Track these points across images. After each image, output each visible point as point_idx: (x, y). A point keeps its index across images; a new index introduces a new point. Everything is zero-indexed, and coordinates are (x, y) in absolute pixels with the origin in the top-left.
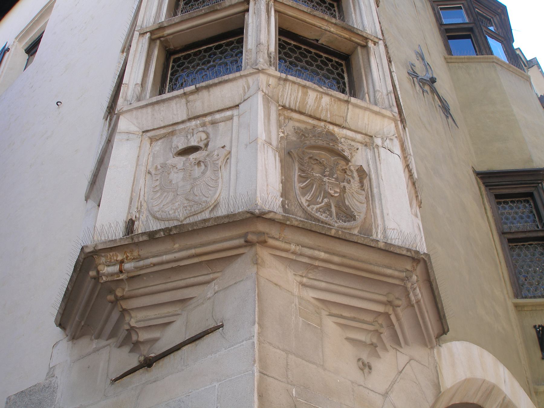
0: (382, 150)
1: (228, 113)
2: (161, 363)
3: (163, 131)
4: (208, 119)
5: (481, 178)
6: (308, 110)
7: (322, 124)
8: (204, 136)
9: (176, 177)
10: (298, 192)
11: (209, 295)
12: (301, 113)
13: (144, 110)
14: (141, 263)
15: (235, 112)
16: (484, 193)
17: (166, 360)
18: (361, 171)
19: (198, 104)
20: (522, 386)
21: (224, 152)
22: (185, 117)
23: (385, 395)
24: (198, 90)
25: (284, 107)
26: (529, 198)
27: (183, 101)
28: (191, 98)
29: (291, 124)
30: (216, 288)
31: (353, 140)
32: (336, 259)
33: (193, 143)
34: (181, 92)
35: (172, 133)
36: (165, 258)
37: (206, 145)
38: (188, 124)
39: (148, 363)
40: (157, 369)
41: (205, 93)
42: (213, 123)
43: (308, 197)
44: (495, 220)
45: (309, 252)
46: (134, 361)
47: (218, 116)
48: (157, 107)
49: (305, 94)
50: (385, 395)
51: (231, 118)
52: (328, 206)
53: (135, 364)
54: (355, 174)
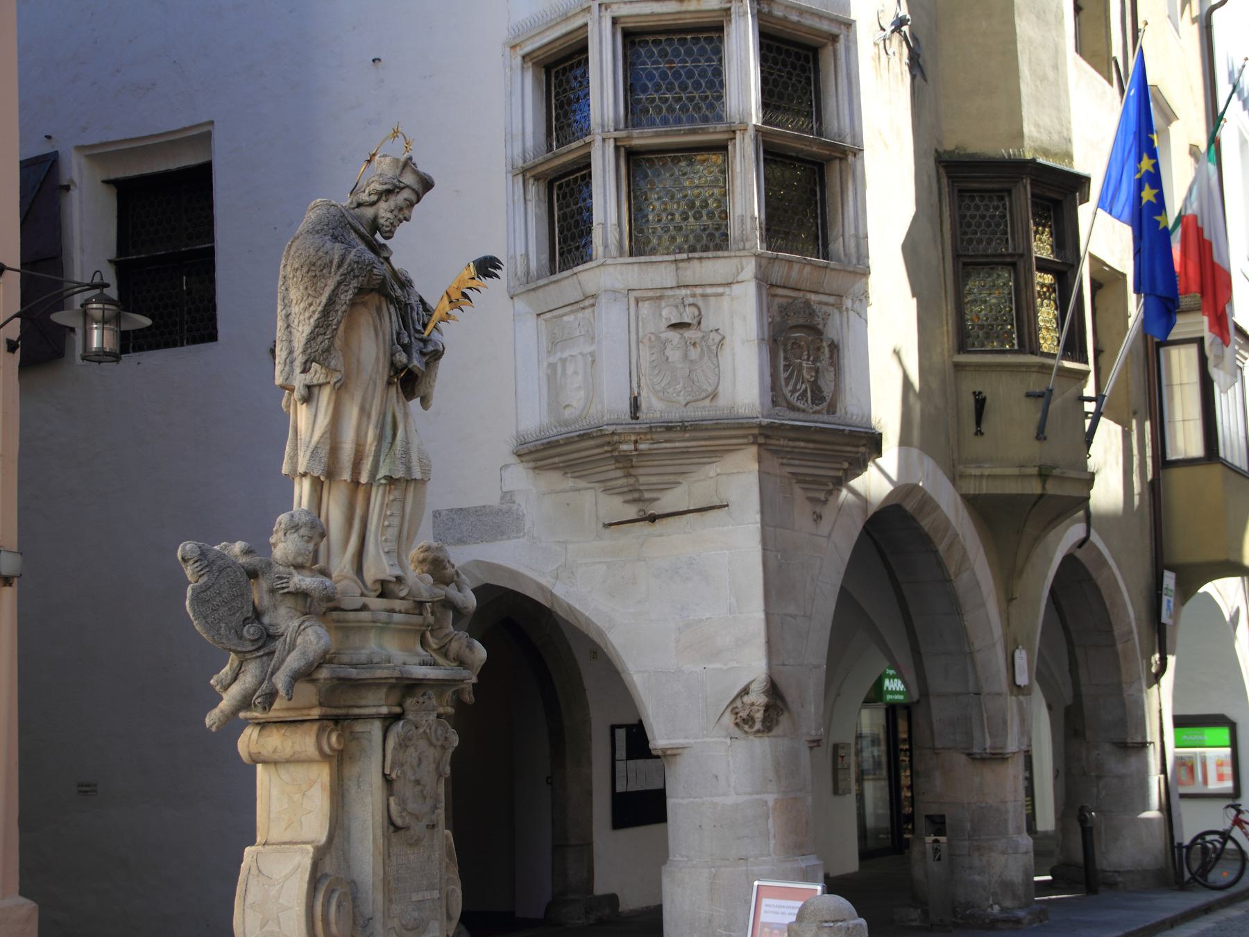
0: (851, 313)
1: (720, 290)
2: (665, 521)
3: (650, 294)
4: (699, 291)
5: (945, 167)
6: (792, 284)
7: (801, 294)
8: (696, 313)
9: (674, 355)
10: (783, 383)
11: (712, 474)
12: (784, 287)
13: (630, 267)
14: (655, 446)
15: (727, 290)
16: (946, 190)
17: (670, 520)
19: (689, 273)
20: (945, 473)
21: (718, 338)
22: (674, 284)
23: (829, 536)
24: (689, 259)
25: (772, 285)
26: (1005, 194)
27: (673, 266)
28: (681, 265)
29: (778, 300)
30: (719, 471)
31: (826, 304)
32: (811, 445)
33: (686, 320)
34: (672, 258)
35: (661, 298)
36: (677, 444)
37: (699, 323)
38: (677, 292)
39: (653, 519)
40: (659, 526)
41: (696, 263)
42: (704, 296)
43: (790, 387)
44: (954, 237)
45: (791, 444)
46: (632, 512)
47: (709, 290)
48: (644, 266)
49: (790, 268)
50: (829, 536)
51: (721, 295)
52: (805, 390)
53: (633, 516)
54: (827, 350)
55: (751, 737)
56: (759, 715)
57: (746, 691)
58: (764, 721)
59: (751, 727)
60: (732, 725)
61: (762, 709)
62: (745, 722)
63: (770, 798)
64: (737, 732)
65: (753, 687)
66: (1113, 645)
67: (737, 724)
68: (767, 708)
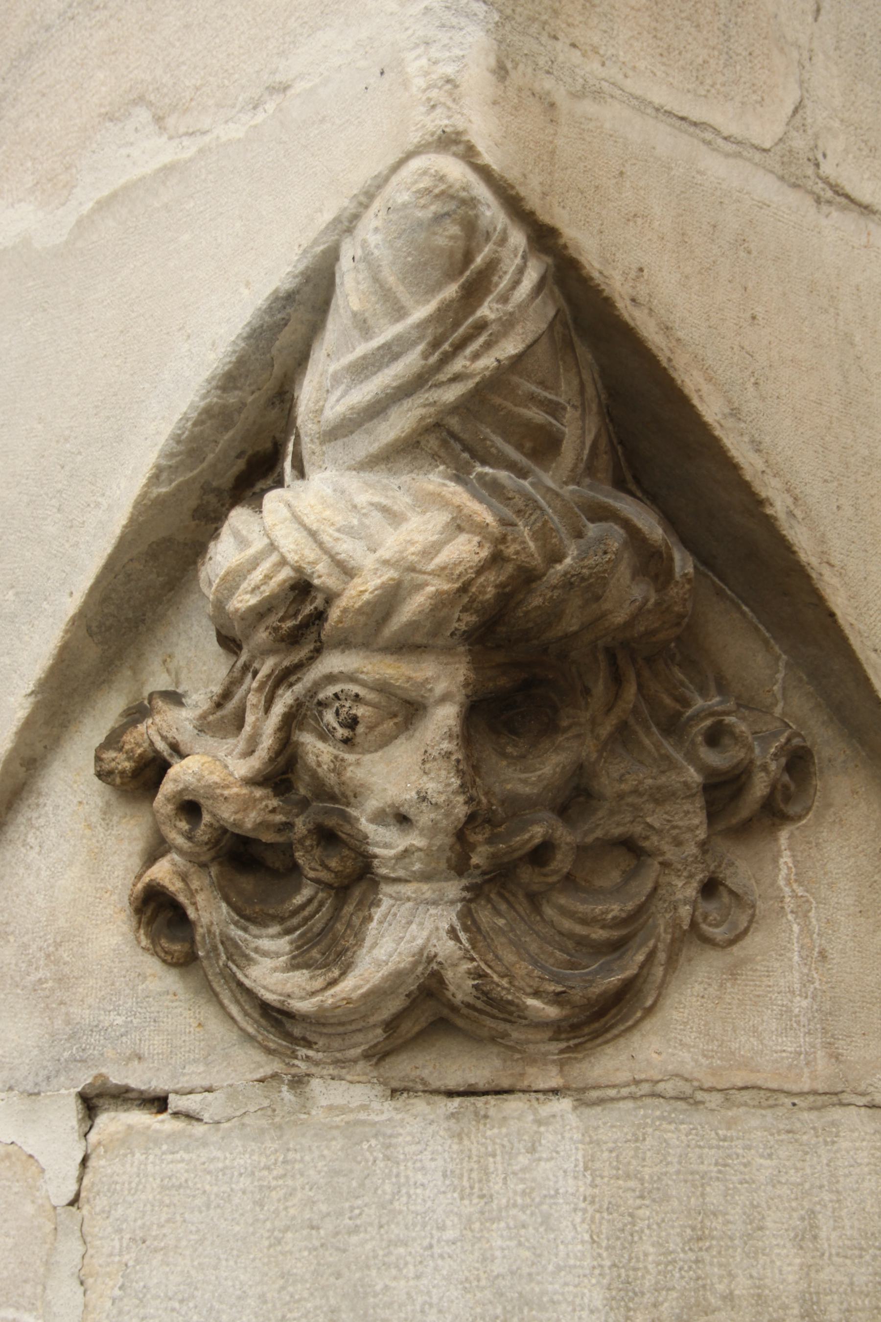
55: (342, 1095)
56: (403, 779)
57: (245, 450)
58: (496, 864)
59: (324, 948)
60: (112, 936)
61: (443, 682)
62: (258, 869)
64: (161, 1025)
65: (323, 394)
67: (159, 912)
68: (518, 661)
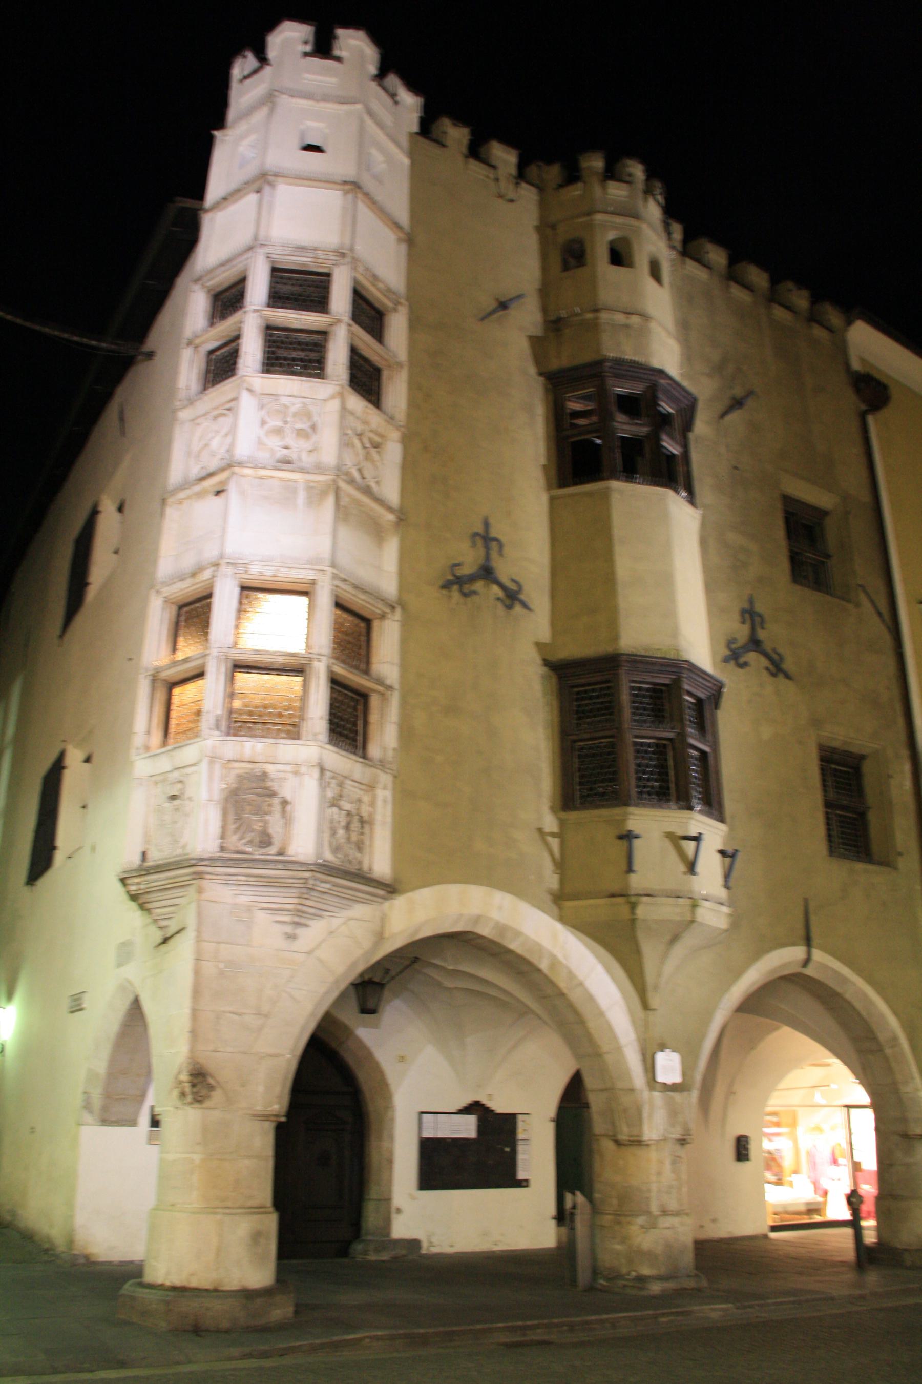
6: (247, 758)
18: (285, 803)
40: (171, 942)
63: (197, 1158)
66: (881, 1050)
